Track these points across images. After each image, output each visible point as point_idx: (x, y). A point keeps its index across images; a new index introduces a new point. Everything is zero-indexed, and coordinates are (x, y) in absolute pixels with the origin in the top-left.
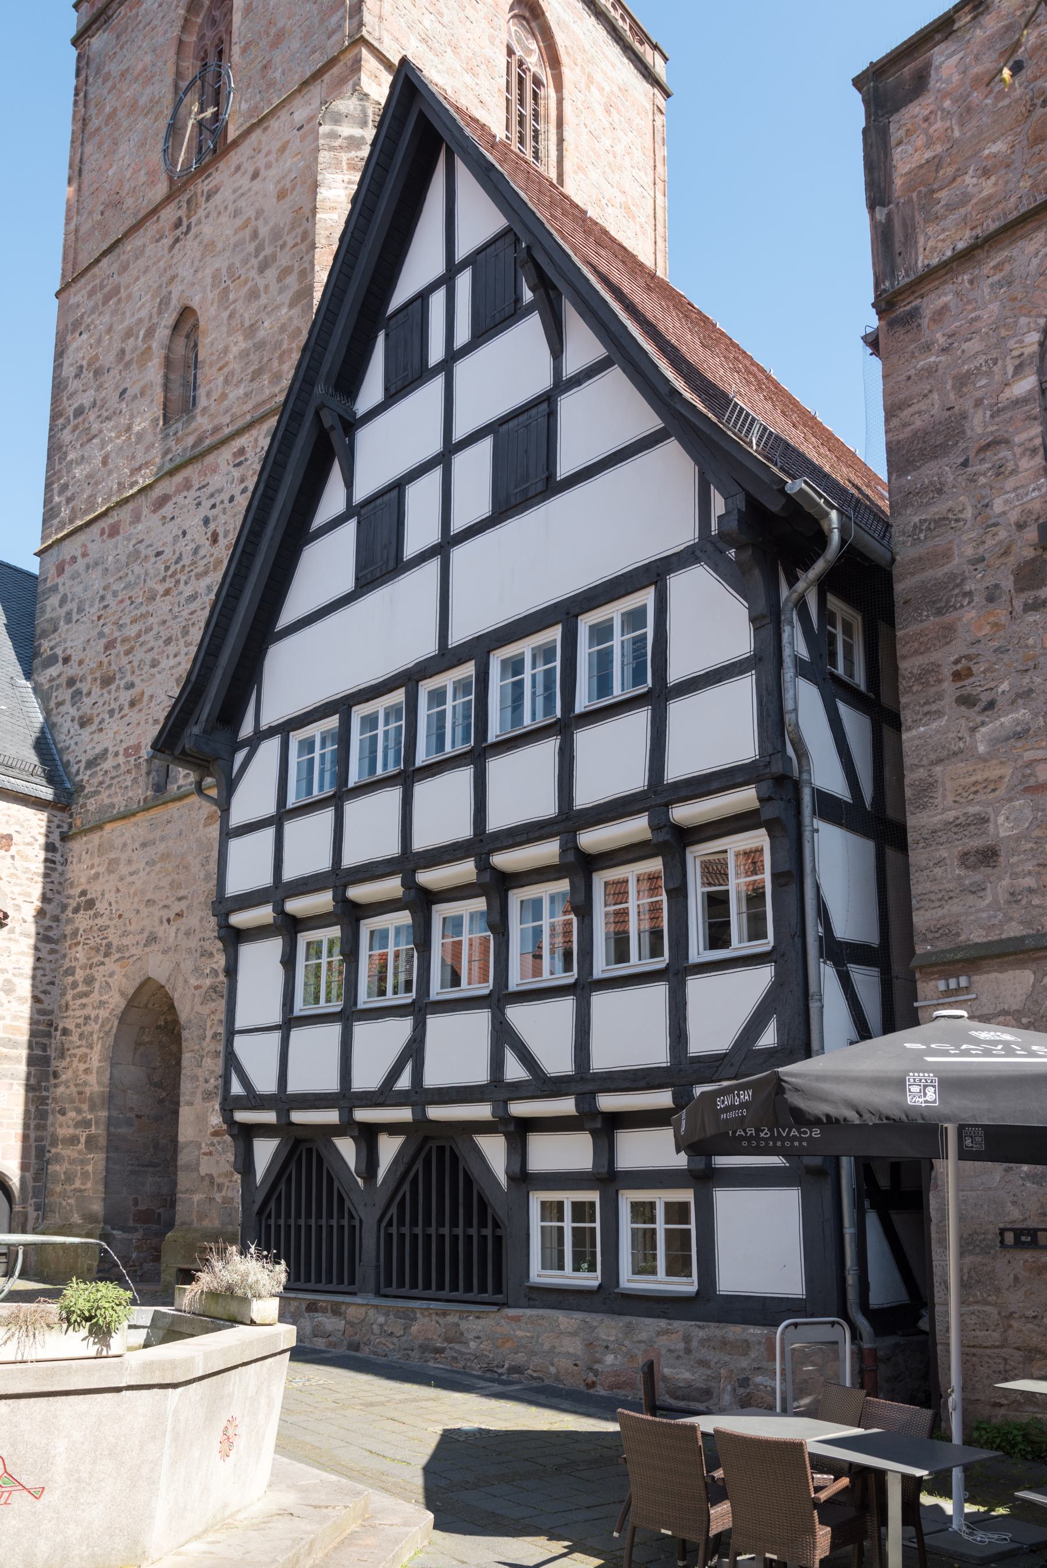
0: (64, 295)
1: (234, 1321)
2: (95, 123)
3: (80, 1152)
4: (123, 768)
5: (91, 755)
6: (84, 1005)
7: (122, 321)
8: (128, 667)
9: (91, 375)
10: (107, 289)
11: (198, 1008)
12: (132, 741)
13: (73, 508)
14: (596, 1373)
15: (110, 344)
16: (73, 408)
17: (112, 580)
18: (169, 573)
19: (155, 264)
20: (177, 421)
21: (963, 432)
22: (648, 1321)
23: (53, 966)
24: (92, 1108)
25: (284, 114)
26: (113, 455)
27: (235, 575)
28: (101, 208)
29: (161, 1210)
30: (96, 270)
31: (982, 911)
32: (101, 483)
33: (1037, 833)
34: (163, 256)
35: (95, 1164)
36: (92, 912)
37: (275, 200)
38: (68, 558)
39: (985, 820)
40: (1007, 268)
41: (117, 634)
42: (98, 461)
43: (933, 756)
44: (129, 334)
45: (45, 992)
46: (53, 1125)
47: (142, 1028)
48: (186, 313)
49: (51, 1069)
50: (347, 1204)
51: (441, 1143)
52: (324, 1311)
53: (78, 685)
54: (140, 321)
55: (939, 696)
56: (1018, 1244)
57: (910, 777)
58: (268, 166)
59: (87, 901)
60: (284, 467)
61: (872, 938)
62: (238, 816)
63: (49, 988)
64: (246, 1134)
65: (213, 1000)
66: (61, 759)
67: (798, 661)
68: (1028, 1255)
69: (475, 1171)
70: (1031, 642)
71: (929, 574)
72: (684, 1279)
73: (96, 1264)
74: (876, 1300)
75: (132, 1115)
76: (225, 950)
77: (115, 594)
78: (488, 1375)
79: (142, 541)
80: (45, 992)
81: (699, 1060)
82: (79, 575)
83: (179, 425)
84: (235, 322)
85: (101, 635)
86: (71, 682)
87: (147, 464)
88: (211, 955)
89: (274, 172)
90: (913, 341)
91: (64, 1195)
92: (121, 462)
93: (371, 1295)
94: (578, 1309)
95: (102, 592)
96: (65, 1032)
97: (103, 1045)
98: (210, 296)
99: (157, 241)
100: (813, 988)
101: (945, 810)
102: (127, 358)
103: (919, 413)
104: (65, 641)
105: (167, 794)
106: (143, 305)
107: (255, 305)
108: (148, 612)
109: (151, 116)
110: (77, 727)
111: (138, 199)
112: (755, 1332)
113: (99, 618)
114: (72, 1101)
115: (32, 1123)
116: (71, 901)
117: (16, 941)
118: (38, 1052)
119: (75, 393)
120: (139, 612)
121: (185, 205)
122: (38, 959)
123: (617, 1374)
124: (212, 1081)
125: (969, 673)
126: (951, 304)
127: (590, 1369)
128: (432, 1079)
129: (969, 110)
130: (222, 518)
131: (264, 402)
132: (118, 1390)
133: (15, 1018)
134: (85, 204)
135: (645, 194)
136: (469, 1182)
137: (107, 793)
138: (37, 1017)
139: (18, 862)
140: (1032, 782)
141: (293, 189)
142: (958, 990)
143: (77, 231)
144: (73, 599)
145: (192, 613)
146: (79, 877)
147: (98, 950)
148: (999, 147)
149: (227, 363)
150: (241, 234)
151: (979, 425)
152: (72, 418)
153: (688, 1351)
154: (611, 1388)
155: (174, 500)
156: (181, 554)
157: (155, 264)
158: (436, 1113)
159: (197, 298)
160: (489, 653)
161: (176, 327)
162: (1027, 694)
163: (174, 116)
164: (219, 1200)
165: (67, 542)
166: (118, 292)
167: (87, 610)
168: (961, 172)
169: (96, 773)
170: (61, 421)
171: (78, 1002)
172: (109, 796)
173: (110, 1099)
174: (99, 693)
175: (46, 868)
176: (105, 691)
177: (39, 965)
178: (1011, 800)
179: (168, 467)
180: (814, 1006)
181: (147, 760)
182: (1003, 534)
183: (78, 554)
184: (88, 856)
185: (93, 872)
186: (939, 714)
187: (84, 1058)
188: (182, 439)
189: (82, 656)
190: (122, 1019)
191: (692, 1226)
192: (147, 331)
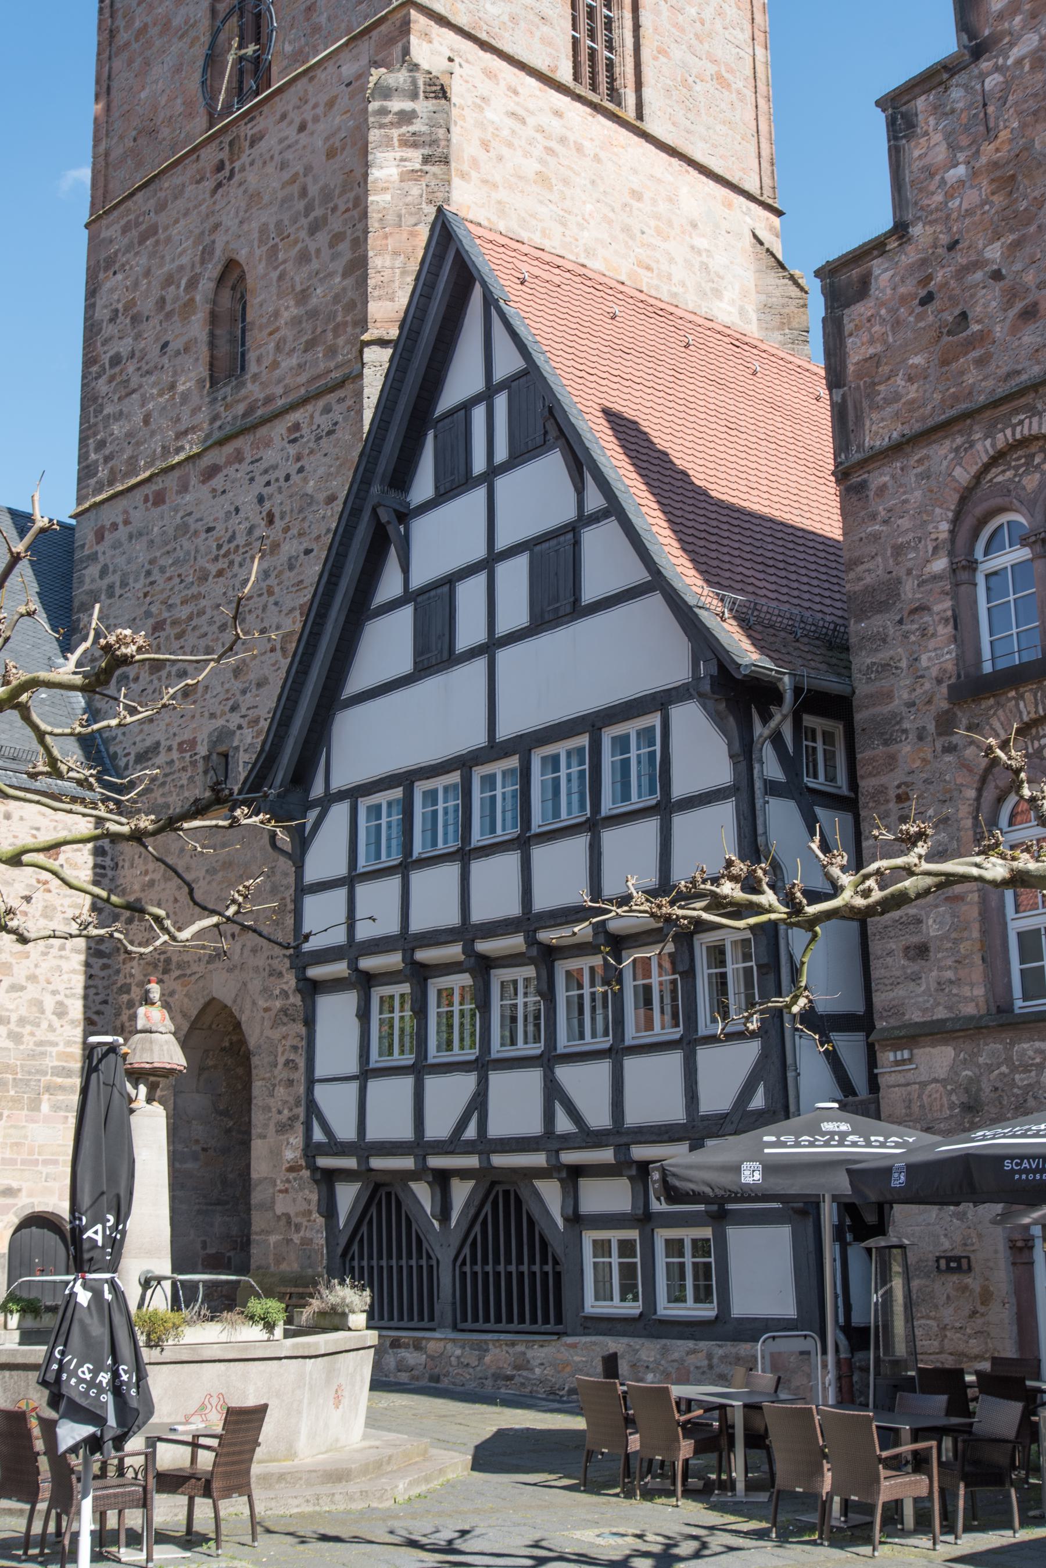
0: (94, 226)
1: (336, 1329)
2: (123, 37)
4: (177, 765)
5: (140, 747)
7: (161, 266)
9: (128, 321)
10: (144, 227)
11: (268, 1033)
12: (187, 736)
13: (112, 468)
15: (148, 290)
16: (109, 355)
17: (158, 554)
18: (222, 552)
19: (196, 207)
20: (225, 385)
21: (899, 595)
22: (680, 1342)
23: (106, 983)
25: (330, 66)
26: (155, 414)
27: (303, 654)
28: (134, 133)
29: (231, 1254)
30: (130, 204)
31: (918, 996)
32: (142, 443)
33: (954, 935)
34: (204, 200)
37: (324, 158)
38: (108, 524)
39: (919, 921)
40: (926, 464)
41: (166, 615)
42: (138, 419)
44: (169, 280)
45: (98, 1013)
47: (206, 1051)
48: (231, 265)
50: (425, 1245)
51: (506, 1187)
52: (406, 1346)
54: (181, 268)
56: (949, 1269)
58: (316, 119)
60: (346, 556)
62: (312, 873)
63: (102, 1008)
64: (328, 1179)
65: (285, 1024)
66: (107, 750)
68: (955, 1278)
69: (537, 1215)
70: (947, 778)
72: (708, 1305)
75: (197, 1148)
77: (162, 570)
78: (551, 1397)
79: (190, 514)
80: (98, 1013)
81: (706, 1118)
82: (121, 544)
83: (228, 389)
85: (148, 614)
87: (193, 429)
88: (280, 975)
89: (322, 127)
90: (863, 508)
92: (164, 423)
93: (449, 1330)
94: (624, 1334)
95: (147, 567)
98: (258, 252)
99: (198, 182)
100: (789, 1060)
102: (168, 308)
103: (869, 570)
106: (184, 251)
107: (306, 269)
108: (200, 594)
109: (187, 40)
111: (174, 130)
113: (146, 595)
117: (67, 958)
119: (111, 338)
120: (189, 592)
121: (227, 148)
124: (286, 1112)
126: (889, 485)
128: (496, 1129)
129: (898, 322)
130: (278, 498)
131: (319, 377)
132: (280, 1359)
133: (68, 1043)
134: (116, 126)
135: (742, 54)
136: (531, 1223)
137: (161, 791)
141: (343, 149)
142: (903, 1062)
143: (107, 155)
144: (114, 572)
147: (156, 966)
148: (917, 360)
149: (277, 329)
151: (909, 590)
152: (107, 366)
153: (711, 1367)
155: (225, 472)
156: (234, 533)
157: (196, 207)
158: (499, 1160)
159: (243, 252)
160: (530, 750)
161: (221, 280)
163: (212, 46)
164: (297, 1242)
165: (106, 505)
166: (156, 233)
167: (132, 585)
168: (893, 374)
170: (95, 369)
172: (163, 795)
174: (148, 679)
175: (95, 874)
176: (154, 677)
177: (91, 983)
178: (936, 906)
179: (217, 435)
180: (790, 1075)
181: (204, 758)
182: (927, 686)
183: (120, 520)
184: (141, 861)
185: (147, 878)
188: (231, 406)
192: (189, 280)
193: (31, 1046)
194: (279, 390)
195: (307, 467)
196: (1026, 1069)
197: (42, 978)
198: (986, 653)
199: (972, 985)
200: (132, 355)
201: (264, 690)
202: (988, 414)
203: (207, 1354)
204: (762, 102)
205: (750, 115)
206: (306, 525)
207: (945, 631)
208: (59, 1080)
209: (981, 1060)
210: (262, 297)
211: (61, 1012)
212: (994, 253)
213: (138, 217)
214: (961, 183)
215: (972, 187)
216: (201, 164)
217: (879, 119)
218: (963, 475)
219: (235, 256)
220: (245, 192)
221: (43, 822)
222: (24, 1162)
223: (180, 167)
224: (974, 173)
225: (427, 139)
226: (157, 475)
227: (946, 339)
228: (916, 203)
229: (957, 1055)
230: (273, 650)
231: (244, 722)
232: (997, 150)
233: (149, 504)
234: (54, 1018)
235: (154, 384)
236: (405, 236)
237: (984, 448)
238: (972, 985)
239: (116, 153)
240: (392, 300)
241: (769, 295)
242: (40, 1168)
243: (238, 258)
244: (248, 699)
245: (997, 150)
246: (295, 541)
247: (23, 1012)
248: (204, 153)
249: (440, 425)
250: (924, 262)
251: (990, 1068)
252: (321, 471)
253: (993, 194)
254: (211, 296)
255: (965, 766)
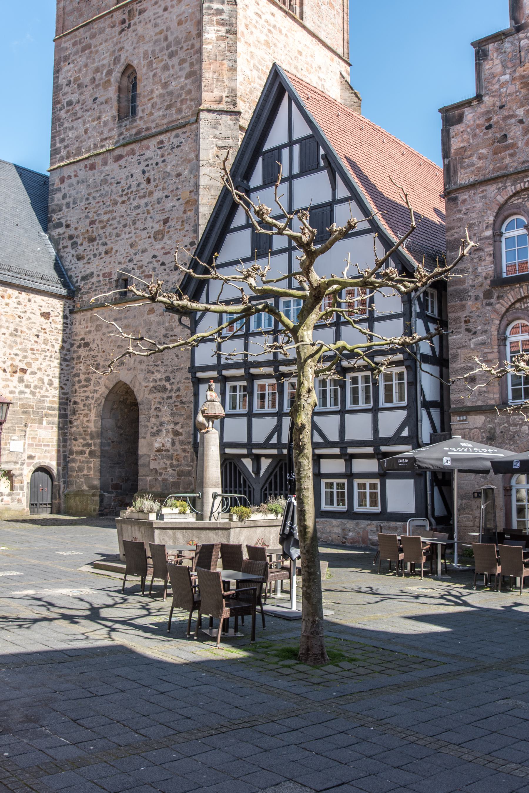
0: (58, 41)
3: (86, 458)
4: (102, 283)
5: (84, 274)
6: (85, 391)
7: (93, 63)
8: (103, 235)
9: (76, 86)
10: (84, 44)
11: (147, 396)
12: (107, 270)
13: (68, 151)
14: (346, 539)
15: (86, 73)
16: (66, 100)
17: (92, 191)
18: (124, 193)
19: (111, 39)
20: (126, 120)
22: (364, 521)
23: (68, 372)
24: (92, 438)
26: (90, 129)
30: (76, 33)
34: (115, 36)
35: (94, 463)
36: (88, 349)
40: (485, 193)
41: (96, 218)
42: (82, 131)
43: (458, 346)
44: (97, 70)
45: (65, 384)
46: (70, 445)
47: (114, 402)
49: (68, 420)
50: (247, 483)
53: (75, 239)
54: (103, 65)
55: (460, 327)
57: (451, 352)
58: (173, 6)
59: (85, 343)
61: (438, 399)
63: (66, 382)
66: (67, 274)
67: (417, 313)
71: (458, 287)
73: (98, 508)
74: (437, 514)
75: (109, 441)
76: (193, 386)
79: (108, 175)
80: (65, 384)
82: (73, 185)
83: (128, 122)
84: (157, 79)
85: (87, 217)
86: (71, 237)
87: (110, 138)
89: (176, 10)
91: (78, 477)
92: (95, 134)
94: (339, 518)
95: (86, 196)
96: (75, 403)
97: (97, 410)
98: (143, 63)
99: (112, 27)
100: (419, 419)
101: (461, 364)
104: (66, 216)
105: (127, 298)
106: (105, 58)
107: (167, 73)
110: (75, 259)
112: (399, 524)
113: (86, 208)
114: (81, 435)
115: (61, 444)
116: (76, 342)
117: (53, 361)
118: (63, 412)
120: (108, 209)
121: (127, 14)
122: (62, 369)
123: (353, 539)
124: (155, 428)
125: (469, 322)
127: (344, 537)
130: (152, 172)
131: (173, 121)
133: (54, 397)
138: (62, 396)
139: (53, 325)
140: (486, 359)
141: (186, 21)
142: (463, 420)
143: (64, 8)
144: (70, 197)
145: (137, 214)
146: (80, 331)
148: (483, 151)
149: (153, 98)
150: (158, 37)
154: (351, 543)
155: (126, 158)
156: (130, 185)
157: (111, 39)
161: (123, 73)
162: (486, 331)
165: (65, 167)
166: (90, 48)
167: (79, 203)
169: (87, 283)
170: (59, 106)
171: (82, 389)
173: (101, 434)
175: (64, 327)
176: (90, 244)
179: (122, 142)
180: (419, 424)
182: (480, 279)
183: (72, 174)
186: (460, 333)
187: (86, 415)
189: (77, 225)
190: (106, 399)
191: (346, 490)
193: (39, 397)
194: (153, 125)
195: (167, 160)
196: (515, 425)
197: (43, 369)
198: (504, 269)
199: (494, 394)
200: (78, 102)
201: (145, 254)
202: (514, 176)
203: (259, 524)
204: (345, 16)
205: (341, 21)
206: (166, 185)
207: (489, 259)
208: (50, 412)
209: (496, 421)
210: (145, 83)
211: (51, 384)
212: (520, 112)
213: (80, 40)
214: (507, 82)
215: (512, 84)
216: (114, 19)
217: (473, 50)
218: (501, 199)
219: (131, 63)
220: (136, 35)
221: (43, 304)
222: (36, 445)
223: (103, 19)
224: (513, 79)
225: (228, 22)
226: (92, 156)
227: (496, 144)
228: (486, 88)
229: (486, 419)
230: (149, 237)
231: (135, 267)
232: (524, 71)
233: (87, 169)
234: (48, 386)
235: (90, 116)
236: (218, 65)
237: (511, 189)
238: (494, 394)
239: (69, 8)
240: (212, 92)
241: (346, 100)
242: (43, 447)
243: (132, 64)
244: (138, 257)
245: (524, 71)
246: (161, 192)
247: (36, 383)
248: (115, 14)
249: (266, 155)
250: (488, 112)
251: (500, 424)
252: (174, 162)
253: (521, 88)
254: (119, 79)
255: (495, 311)
